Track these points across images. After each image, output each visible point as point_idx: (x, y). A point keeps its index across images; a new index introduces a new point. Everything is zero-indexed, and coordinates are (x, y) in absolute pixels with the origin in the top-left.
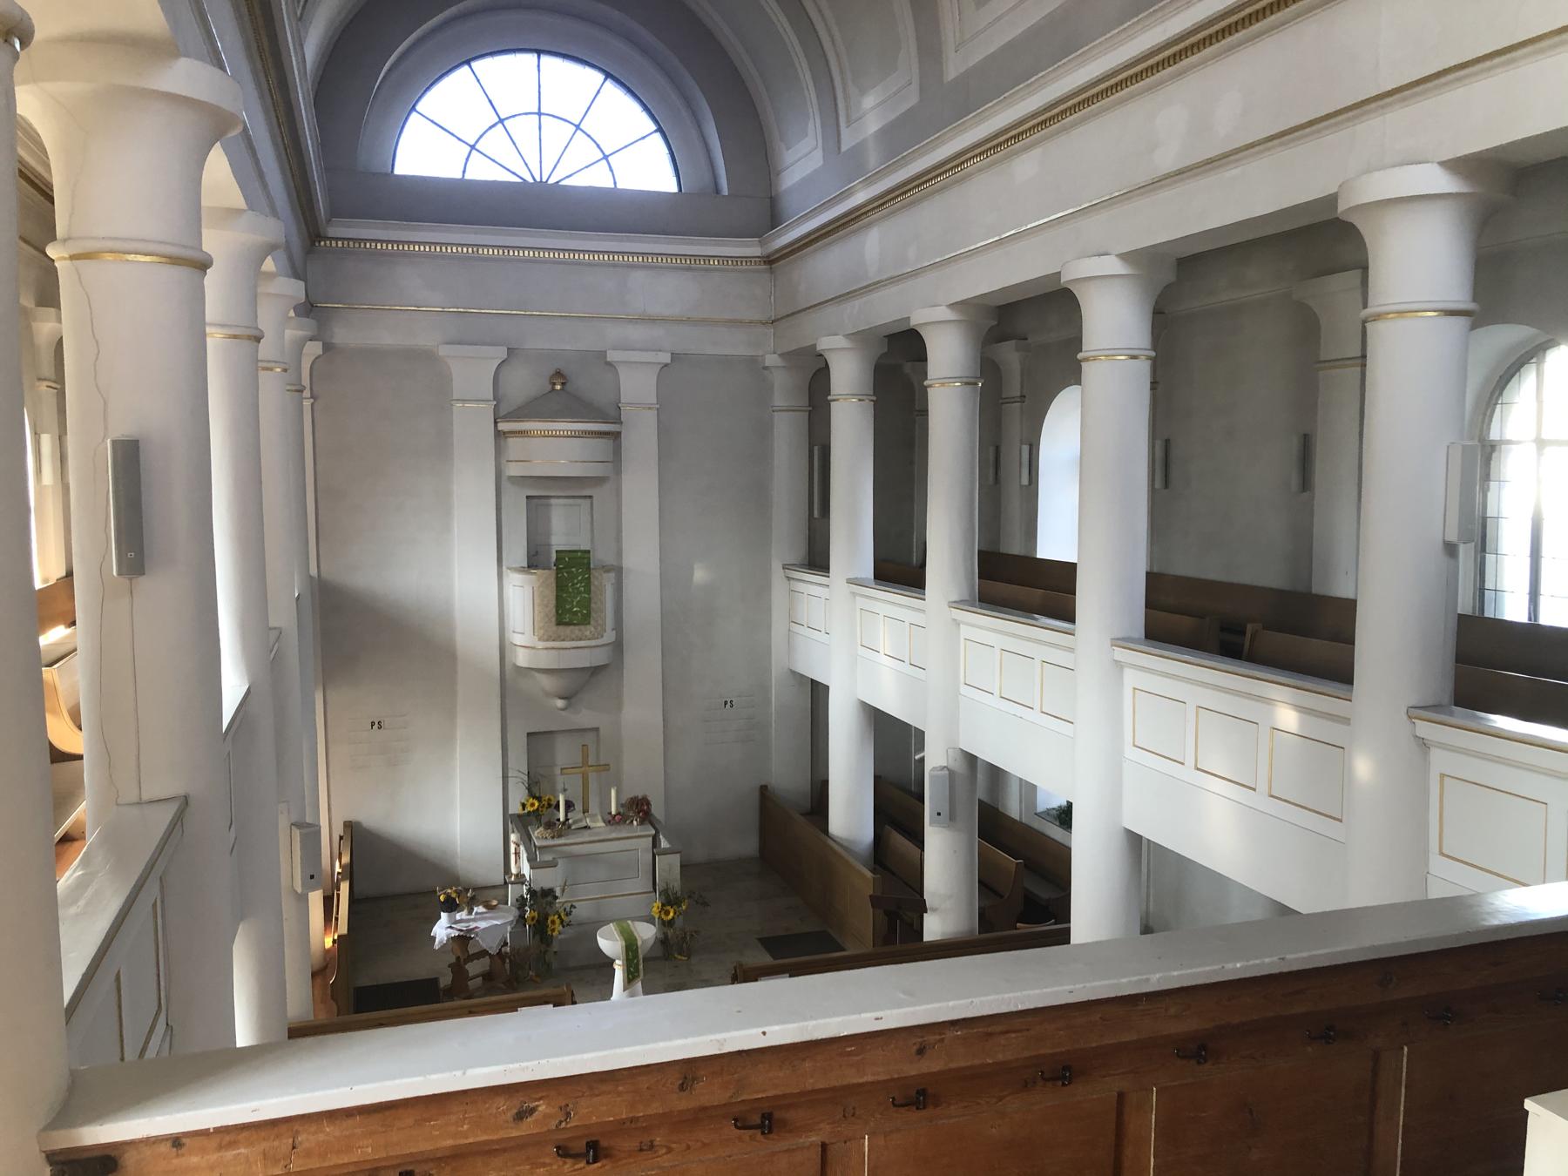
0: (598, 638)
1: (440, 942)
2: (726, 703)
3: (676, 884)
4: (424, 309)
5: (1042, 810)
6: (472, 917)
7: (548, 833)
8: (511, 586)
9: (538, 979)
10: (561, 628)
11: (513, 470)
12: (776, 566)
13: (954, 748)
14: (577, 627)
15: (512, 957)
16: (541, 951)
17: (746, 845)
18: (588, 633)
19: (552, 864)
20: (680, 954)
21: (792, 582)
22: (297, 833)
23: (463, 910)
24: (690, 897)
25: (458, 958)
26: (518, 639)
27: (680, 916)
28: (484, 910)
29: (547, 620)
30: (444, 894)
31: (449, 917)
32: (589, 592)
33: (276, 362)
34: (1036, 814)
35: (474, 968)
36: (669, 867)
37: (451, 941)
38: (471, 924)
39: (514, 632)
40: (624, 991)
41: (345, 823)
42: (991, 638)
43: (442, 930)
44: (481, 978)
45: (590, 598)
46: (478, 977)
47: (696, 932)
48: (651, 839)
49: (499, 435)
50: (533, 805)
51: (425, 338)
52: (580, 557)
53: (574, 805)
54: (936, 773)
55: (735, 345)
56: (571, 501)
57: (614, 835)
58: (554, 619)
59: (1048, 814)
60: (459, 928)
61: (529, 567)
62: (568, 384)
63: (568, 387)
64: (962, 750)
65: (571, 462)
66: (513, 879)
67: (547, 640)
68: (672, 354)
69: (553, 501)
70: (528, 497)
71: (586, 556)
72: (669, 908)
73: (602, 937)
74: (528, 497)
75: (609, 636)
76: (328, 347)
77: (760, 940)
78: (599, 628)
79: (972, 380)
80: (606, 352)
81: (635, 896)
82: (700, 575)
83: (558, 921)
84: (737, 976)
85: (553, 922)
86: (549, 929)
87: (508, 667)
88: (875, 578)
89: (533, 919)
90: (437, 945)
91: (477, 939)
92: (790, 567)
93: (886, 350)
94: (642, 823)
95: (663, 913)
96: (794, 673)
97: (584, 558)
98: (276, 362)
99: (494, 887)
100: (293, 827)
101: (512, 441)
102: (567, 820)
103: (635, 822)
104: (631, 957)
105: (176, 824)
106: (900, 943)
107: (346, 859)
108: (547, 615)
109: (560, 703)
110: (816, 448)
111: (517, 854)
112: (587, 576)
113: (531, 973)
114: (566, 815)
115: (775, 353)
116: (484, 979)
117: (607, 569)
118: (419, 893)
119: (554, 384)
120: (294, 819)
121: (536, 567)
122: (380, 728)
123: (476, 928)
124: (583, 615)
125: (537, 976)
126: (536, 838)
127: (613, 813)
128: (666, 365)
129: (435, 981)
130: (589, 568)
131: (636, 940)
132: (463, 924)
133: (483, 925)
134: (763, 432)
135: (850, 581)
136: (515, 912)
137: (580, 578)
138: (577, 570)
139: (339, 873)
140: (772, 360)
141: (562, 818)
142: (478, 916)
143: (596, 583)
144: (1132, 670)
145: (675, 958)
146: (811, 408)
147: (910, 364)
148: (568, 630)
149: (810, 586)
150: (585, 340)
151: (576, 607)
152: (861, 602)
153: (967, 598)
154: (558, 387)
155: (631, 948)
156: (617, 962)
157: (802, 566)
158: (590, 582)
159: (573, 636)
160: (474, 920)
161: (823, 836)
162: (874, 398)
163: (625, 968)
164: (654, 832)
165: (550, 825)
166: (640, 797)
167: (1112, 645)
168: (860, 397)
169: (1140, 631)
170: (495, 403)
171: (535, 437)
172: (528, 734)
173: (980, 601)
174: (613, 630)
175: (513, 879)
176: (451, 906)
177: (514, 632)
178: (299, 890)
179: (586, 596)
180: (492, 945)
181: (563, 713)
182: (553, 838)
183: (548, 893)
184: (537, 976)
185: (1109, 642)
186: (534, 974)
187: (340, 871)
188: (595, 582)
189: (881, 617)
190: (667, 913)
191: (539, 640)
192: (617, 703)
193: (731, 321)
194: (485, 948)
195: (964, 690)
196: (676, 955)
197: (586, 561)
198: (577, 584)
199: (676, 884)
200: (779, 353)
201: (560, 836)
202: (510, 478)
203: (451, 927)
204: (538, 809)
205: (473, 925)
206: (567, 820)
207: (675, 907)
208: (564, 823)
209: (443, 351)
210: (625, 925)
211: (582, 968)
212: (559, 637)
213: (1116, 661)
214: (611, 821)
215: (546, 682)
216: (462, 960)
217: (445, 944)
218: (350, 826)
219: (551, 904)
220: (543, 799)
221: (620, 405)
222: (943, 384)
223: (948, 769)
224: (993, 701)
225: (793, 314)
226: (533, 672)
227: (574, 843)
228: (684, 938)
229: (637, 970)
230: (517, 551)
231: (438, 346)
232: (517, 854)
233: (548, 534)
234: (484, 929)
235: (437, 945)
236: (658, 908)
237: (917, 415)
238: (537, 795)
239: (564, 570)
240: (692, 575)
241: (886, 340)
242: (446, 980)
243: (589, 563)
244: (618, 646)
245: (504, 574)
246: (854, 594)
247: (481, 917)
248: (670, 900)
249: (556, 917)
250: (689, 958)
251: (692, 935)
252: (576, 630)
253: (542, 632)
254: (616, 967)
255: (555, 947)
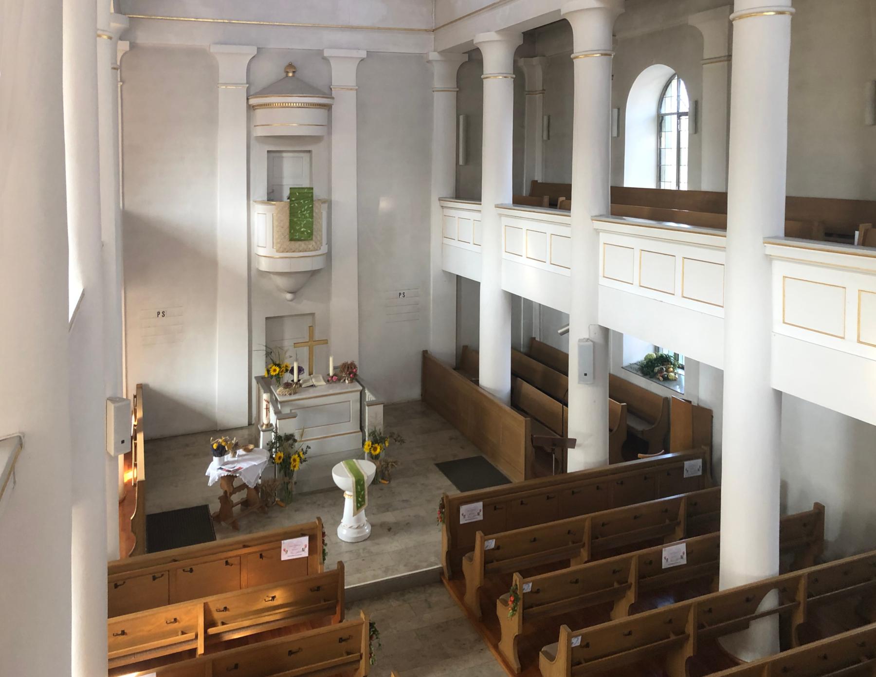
0: (317, 250)
1: (212, 481)
2: (400, 294)
3: (380, 427)
4: (201, 20)
5: (626, 365)
6: (236, 459)
7: (287, 391)
8: (256, 213)
9: (283, 504)
10: (293, 242)
11: (259, 132)
12: (434, 198)
13: (594, 325)
14: (303, 242)
15: (264, 488)
16: (284, 482)
17: (415, 392)
18: (310, 246)
19: (293, 416)
20: (383, 479)
21: (445, 210)
22: (111, 407)
23: (229, 453)
24: (391, 437)
25: (226, 492)
26: (261, 252)
27: (384, 451)
28: (244, 453)
29: (283, 237)
30: (217, 442)
31: (220, 460)
32: (312, 217)
33: (103, 30)
34: (622, 368)
35: (236, 498)
36: (374, 416)
37: (220, 479)
38: (235, 465)
39: (258, 246)
40: (353, 516)
41: (137, 385)
42: (638, 244)
43: (215, 470)
44: (240, 505)
45: (313, 222)
46: (239, 504)
47: (394, 462)
48: (359, 393)
49: (251, 108)
50: (275, 370)
51: (200, 40)
52: (306, 193)
53: (303, 370)
54: (582, 344)
55: (406, 46)
56: (296, 154)
57: (331, 392)
58: (287, 236)
59: (631, 368)
60: (227, 469)
61: (268, 200)
62: (297, 72)
63: (296, 74)
64: (600, 326)
65: (301, 125)
66: (264, 427)
67: (283, 252)
68: (367, 52)
69: (284, 155)
70: (268, 152)
71: (311, 191)
72: (376, 445)
73: (335, 473)
74: (268, 152)
75: (324, 249)
76: (133, 46)
77: (438, 465)
78: (318, 243)
79: (609, 52)
80: (323, 50)
81: (349, 435)
82: (384, 204)
83: (298, 460)
84: (444, 505)
85: (295, 460)
86: (292, 466)
87: (253, 272)
88: (513, 203)
89: (280, 458)
90: (210, 484)
91: (241, 477)
92: (444, 199)
93: (522, 43)
94: (351, 381)
95: (372, 449)
96: (445, 272)
97: (309, 193)
98: (103, 30)
99: (242, 428)
100: (108, 401)
101: (259, 112)
102: (299, 380)
103: (347, 381)
104: (359, 490)
105: (8, 479)
106: (556, 473)
107: (140, 414)
108: (283, 234)
109: (289, 296)
110: (461, 118)
111: (267, 409)
112: (310, 206)
113: (277, 499)
114: (298, 377)
115: (434, 51)
116: (241, 505)
117: (324, 202)
118: (189, 434)
119: (287, 72)
120: (109, 394)
121: (273, 200)
122: (163, 316)
123: (240, 468)
124: (308, 233)
125: (282, 500)
126: (278, 395)
127: (331, 374)
128: (363, 60)
129: (205, 508)
130: (312, 200)
131: (363, 477)
132: (230, 466)
133: (244, 465)
134: (426, 106)
135: (497, 206)
136: (267, 454)
137: (306, 207)
138: (304, 202)
139: (135, 426)
140: (434, 56)
141: (295, 380)
142: (240, 458)
143: (317, 211)
144: (780, 262)
145: (380, 482)
146: (458, 89)
147: (522, 59)
148: (298, 244)
149: (463, 212)
150: (310, 42)
151: (304, 227)
152: (505, 221)
153: (605, 213)
154: (290, 74)
155: (359, 482)
156: (347, 493)
157: (452, 198)
158: (313, 210)
159: (301, 249)
160: (237, 462)
161: (475, 386)
162: (514, 76)
163: (355, 498)
164: (361, 388)
165: (287, 385)
166: (349, 362)
167: (764, 243)
168: (505, 75)
169: (782, 233)
170: (248, 85)
171: (275, 108)
172: (267, 318)
173: (611, 215)
174: (326, 244)
175: (264, 427)
176: (221, 452)
177: (258, 246)
178: (112, 453)
179: (310, 220)
180: (252, 481)
181: (290, 303)
182: (290, 394)
183: (290, 438)
184: (282, 500)
185: (762, 241)
186: (279, 500)
187: (136, 423)
188: (316, 210)
189: (524, 230)
190: (375, 449)
191: (277, 251)
192: (327, 295)
193: (406, 29)
194: (246, 482)
195: (602, 281)
196: (380, 480)
197: (310, 195)
198: (304, 211)
199: (380, 427)
200: (439, 51)
201: (295, 393)
202: (257, 137)
203: (221, 468)
204: (279, 373)
205: (237, 466)
206: (299, 380)
207: (380, 444)
208: (297, 383)
209: (214, 49)
210: (352, 463)
211: (313, 493)
212: (291, 249)
213: (767, 255)
214: (329, 380)
215: (281, 282)
216: (228, 494)
217: (216, 482)
218: (140, 387)
219: (291, 446)
220: (282, 366)
221: (331, 87)
222: (586, 56)
223: (592, 341)
224: (634, 290)
225: (452, 22)
226: (272, 276)
227: (304, 398)
228: (387, 467)
229: (364, 500)
230: (261, 190)
231: (210, 46)
232: (267, 409)
233: (281, 177)
234: (247, 469)
235: (210, 484)
236: (369, 446)
237: (526, 94)
238: (277, 363)
239: (296, 202)
240: (378, 204)
241: (522, 35)
242: (215, 507)
243: (312, 196)
244: (328, 256)
245: (251, 206)
246: (501, 215)
247: (242, 459)
248: (377, 439)
249: (297, 456)
250: (390, 481)
251: (392, 465)
252: (303, 245)
253: (279, 245)
254: (346, 497)
255: (295, 478)
